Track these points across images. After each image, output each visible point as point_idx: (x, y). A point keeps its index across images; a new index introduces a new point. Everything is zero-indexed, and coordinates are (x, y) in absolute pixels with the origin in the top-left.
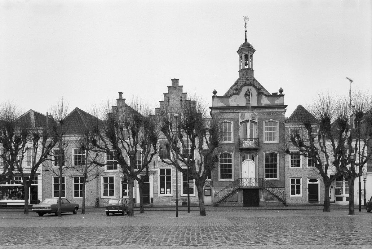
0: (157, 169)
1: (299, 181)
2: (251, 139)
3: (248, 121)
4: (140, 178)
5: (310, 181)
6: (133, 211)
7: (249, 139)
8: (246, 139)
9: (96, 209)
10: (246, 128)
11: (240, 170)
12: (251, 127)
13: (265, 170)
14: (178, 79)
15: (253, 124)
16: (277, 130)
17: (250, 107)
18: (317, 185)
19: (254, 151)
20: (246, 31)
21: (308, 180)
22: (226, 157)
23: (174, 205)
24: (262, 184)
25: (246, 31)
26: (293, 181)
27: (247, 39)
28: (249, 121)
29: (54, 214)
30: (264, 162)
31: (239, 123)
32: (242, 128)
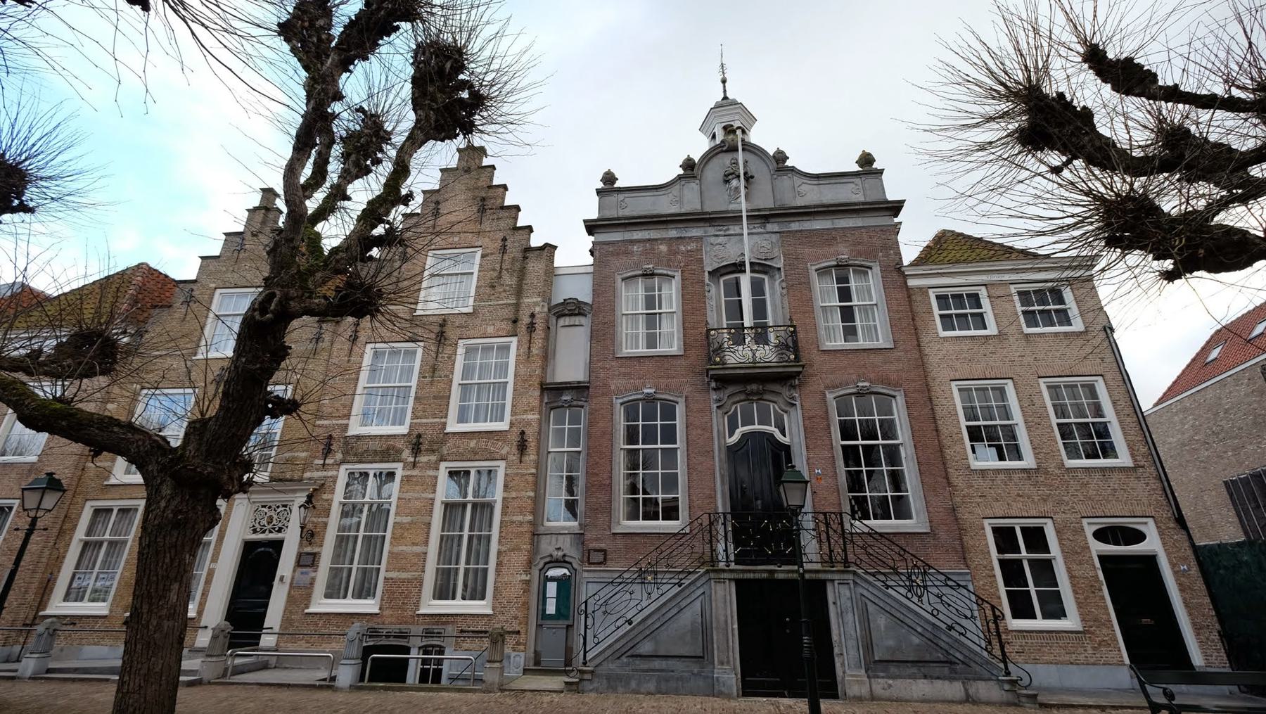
0: (334, 473)
1: (1036, 538)
2: (761, 335)
3: (738, 267)
4: (310, 212)
5: (1101, 535)
6: (1091, 44)
7: (751, 328)
8: (738, 335)
9: (540, 613)
10: (739, 295)
11: (372, 591)
12: (757, 288)
13: (843, 479)
15: (766, 278)
16: (874, 299)
17: (744, 214)
18: (1151, 560)
19: (776, 387)
20: (724, 81)
21: (1089, 531)
22: (650, 416)
23: (1120, 691)
24: (845, 550)
25: (724, 81)
26: (1005, 538)
27: (722, 85)
28: (743, 264)
29: (551, 609)
30: (838, 442)
31: (707, 274)
32: (716, 295)
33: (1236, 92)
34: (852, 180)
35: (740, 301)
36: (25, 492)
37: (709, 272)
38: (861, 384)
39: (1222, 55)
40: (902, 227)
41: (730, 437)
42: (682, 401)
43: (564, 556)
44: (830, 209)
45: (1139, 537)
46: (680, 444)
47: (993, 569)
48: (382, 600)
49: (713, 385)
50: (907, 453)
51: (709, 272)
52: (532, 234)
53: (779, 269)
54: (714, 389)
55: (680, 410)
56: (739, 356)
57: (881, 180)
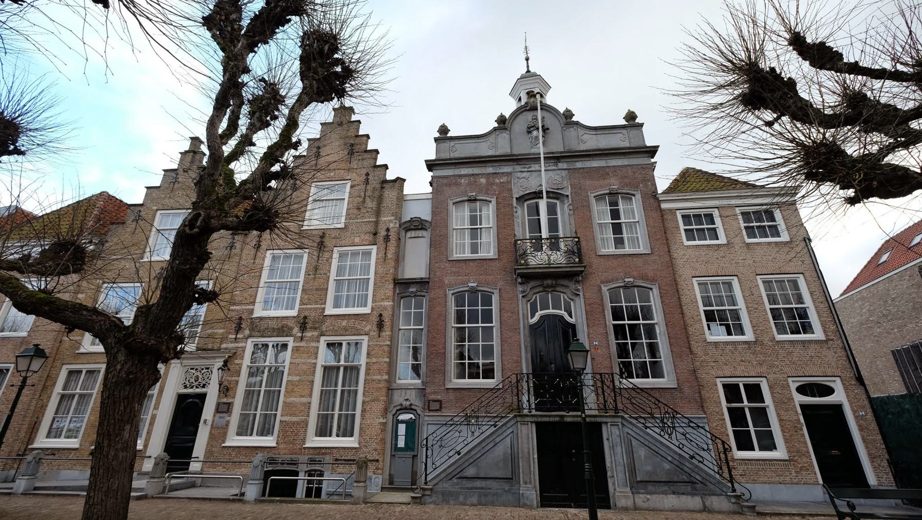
0: (243, 344)
1: (754, 392)
2: (554, 244)
3: (538, 195)
5: (802, 390)
7: (547, 239)
8: (537, 244)
9: (393, 446)
10: (538, 215)
12: (552, 210)
13: (614, 349)
14: (404, 180)
15: (558, 202)
16: (637, 217)
17: (542, 156)
18: (838, 408)
19: (565, 282)
20: (527, 59)
21: (793, 386)
22: (473, 303)
24: (615, 401)
25: (527, 59)
26: (732, 392)
27: (526, 62)
28: (541, 192)
29: (401, 443)
30: (610, 322)
31: (515, 199)
32: (522, 215)
33: (900, 67)
34: (620, 131)
35: (539, 219)
36: (18, 358)
37: (516, 198)
38: (627, 280)
39: (890, 40)
40: (657, 165)
41: (531, 318)
42: (496, 292)
43: (411, 405)
44: (605, 152)
45: (830, 391)
46: (495, 323)
47: (723, 414)
48: (278, 437)
49: (519, 280)
50: (660, 330)
51: (516, 198)
52: (387, 171)
53: (568, 196)
54: (520, 283)
55: (495, 299)
56: (538, 259)
57: (642, 131)
